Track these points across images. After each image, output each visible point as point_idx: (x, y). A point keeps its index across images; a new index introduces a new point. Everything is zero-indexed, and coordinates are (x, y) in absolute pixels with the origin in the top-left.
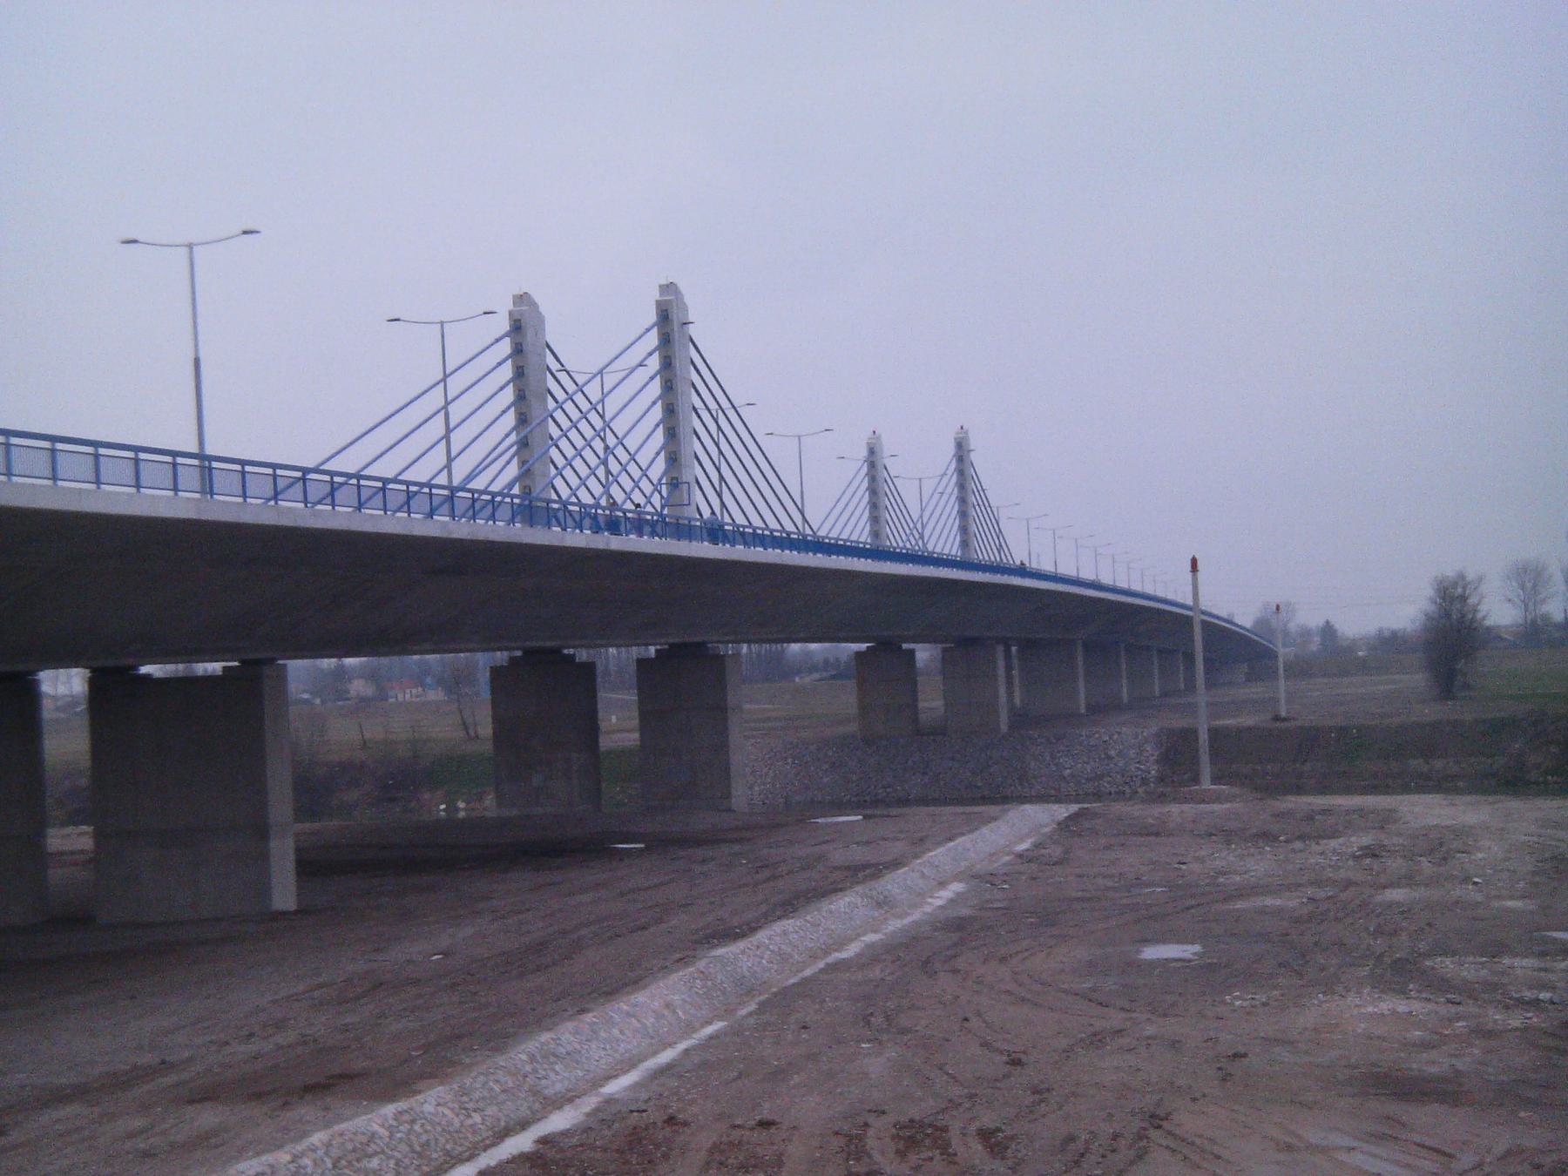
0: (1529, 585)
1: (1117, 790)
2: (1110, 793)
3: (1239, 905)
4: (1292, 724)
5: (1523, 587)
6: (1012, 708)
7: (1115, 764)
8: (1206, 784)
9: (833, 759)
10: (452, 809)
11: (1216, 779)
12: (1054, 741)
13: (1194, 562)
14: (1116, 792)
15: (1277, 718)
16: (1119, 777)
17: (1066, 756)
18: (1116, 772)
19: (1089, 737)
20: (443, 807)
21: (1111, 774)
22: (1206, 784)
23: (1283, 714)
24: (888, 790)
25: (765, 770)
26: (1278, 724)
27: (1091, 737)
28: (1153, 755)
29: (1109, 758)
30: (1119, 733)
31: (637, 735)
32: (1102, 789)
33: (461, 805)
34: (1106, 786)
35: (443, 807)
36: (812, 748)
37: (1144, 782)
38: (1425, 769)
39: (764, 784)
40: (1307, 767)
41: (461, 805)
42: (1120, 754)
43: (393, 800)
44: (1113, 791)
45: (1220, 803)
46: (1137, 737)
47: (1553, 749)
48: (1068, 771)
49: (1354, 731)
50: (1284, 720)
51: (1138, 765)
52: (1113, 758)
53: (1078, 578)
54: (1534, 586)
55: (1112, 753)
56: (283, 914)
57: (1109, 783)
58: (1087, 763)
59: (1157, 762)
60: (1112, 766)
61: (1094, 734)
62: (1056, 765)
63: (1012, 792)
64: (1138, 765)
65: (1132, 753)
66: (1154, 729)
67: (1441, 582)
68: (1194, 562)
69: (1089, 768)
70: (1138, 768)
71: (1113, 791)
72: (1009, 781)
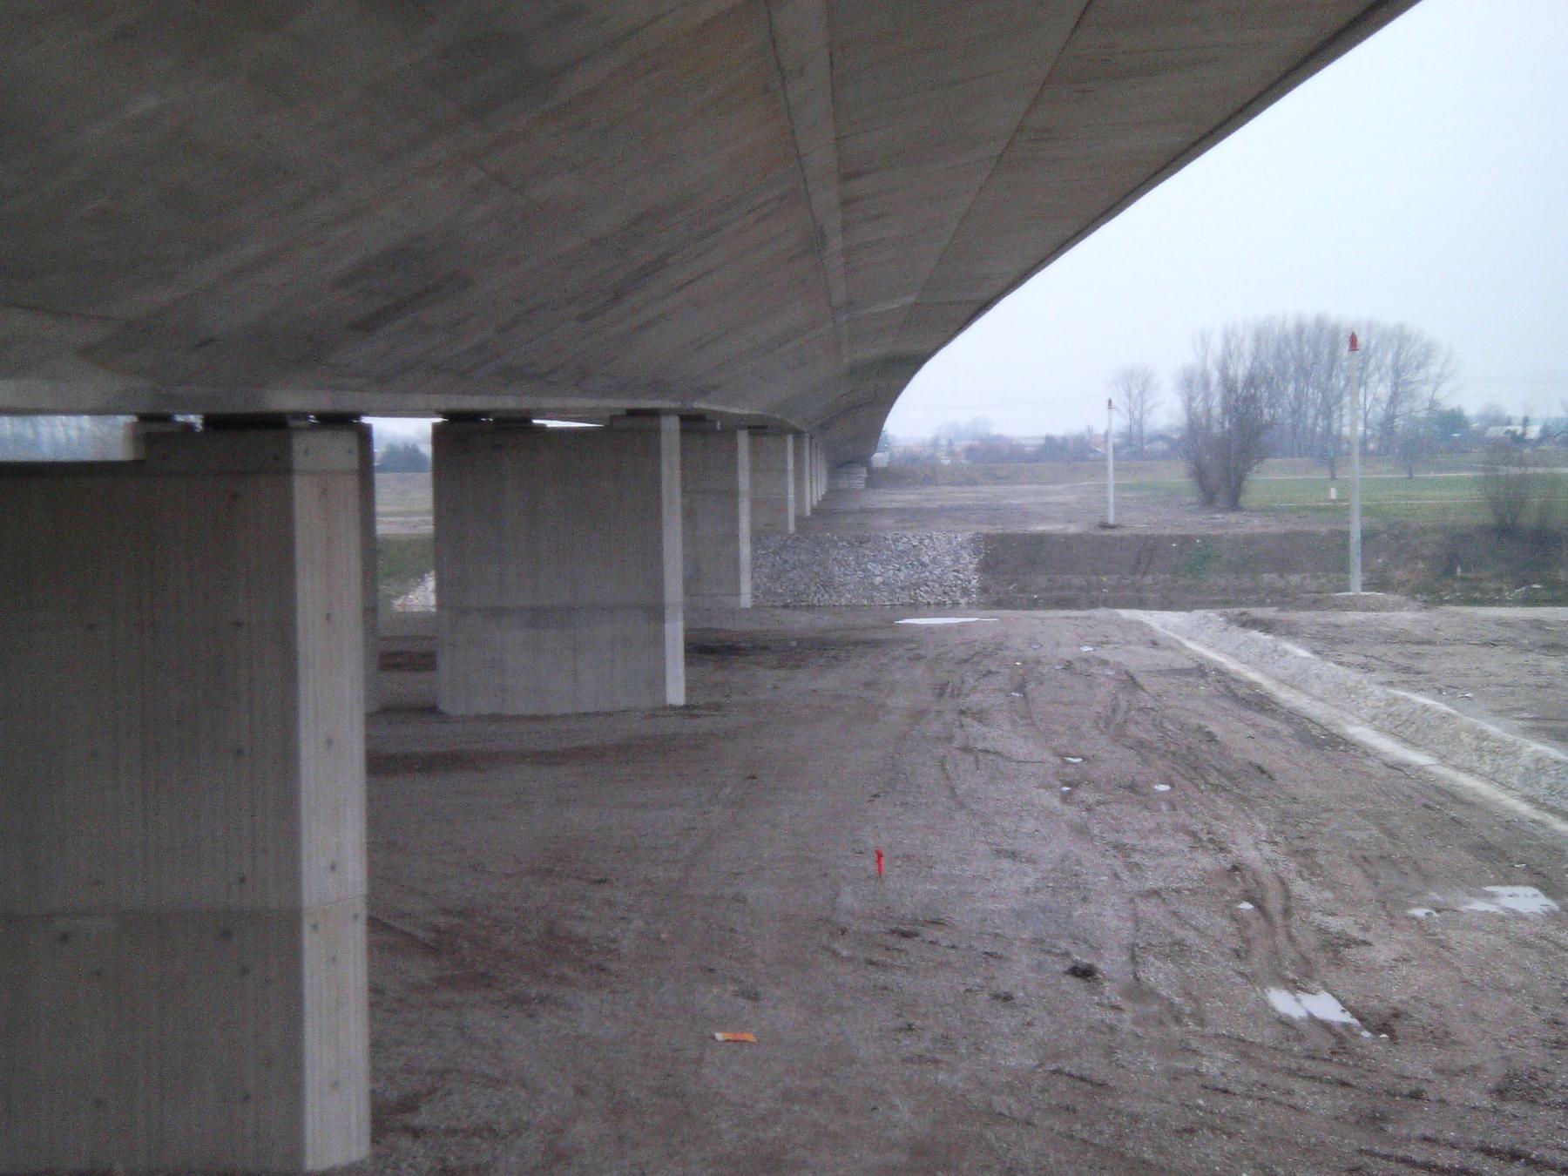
0: (1135, 392)
1: (936, 601)
4: (1117, 533)
5: (1129, 395)
6: (812, 506)
7: (931, 573)
8: (1356, 589)
11: (1367, 586)
15: (1105, 526)
16: (937, 586)
18: (933, 581)
19: (895, 541)
22: (1356, 589)
23: (1111, 521)
29: (923, 565)
30: (930, 538)
31: (431, 527)
32: (920, 598)
34: (924, 598)
37: (966, 592)
38: (1280, 584)
40: (1148, 580)
45: (1388, 611)
47: (1421, 565)
48: (878, 578)
49: (1198, 541)
50: (1113, 527)
52: (928, 565)
54: (1141, 394)
55: (926, 559)
56: (672, 707)
57: (926, 592)
58: (899, 570)
59: (977, 570)
60: (927, 574)
62: (863, 571)
65: (948, 561)
66: (969, 535)
69: (902, 576)
70: (956, 577)
71: (932, 601)
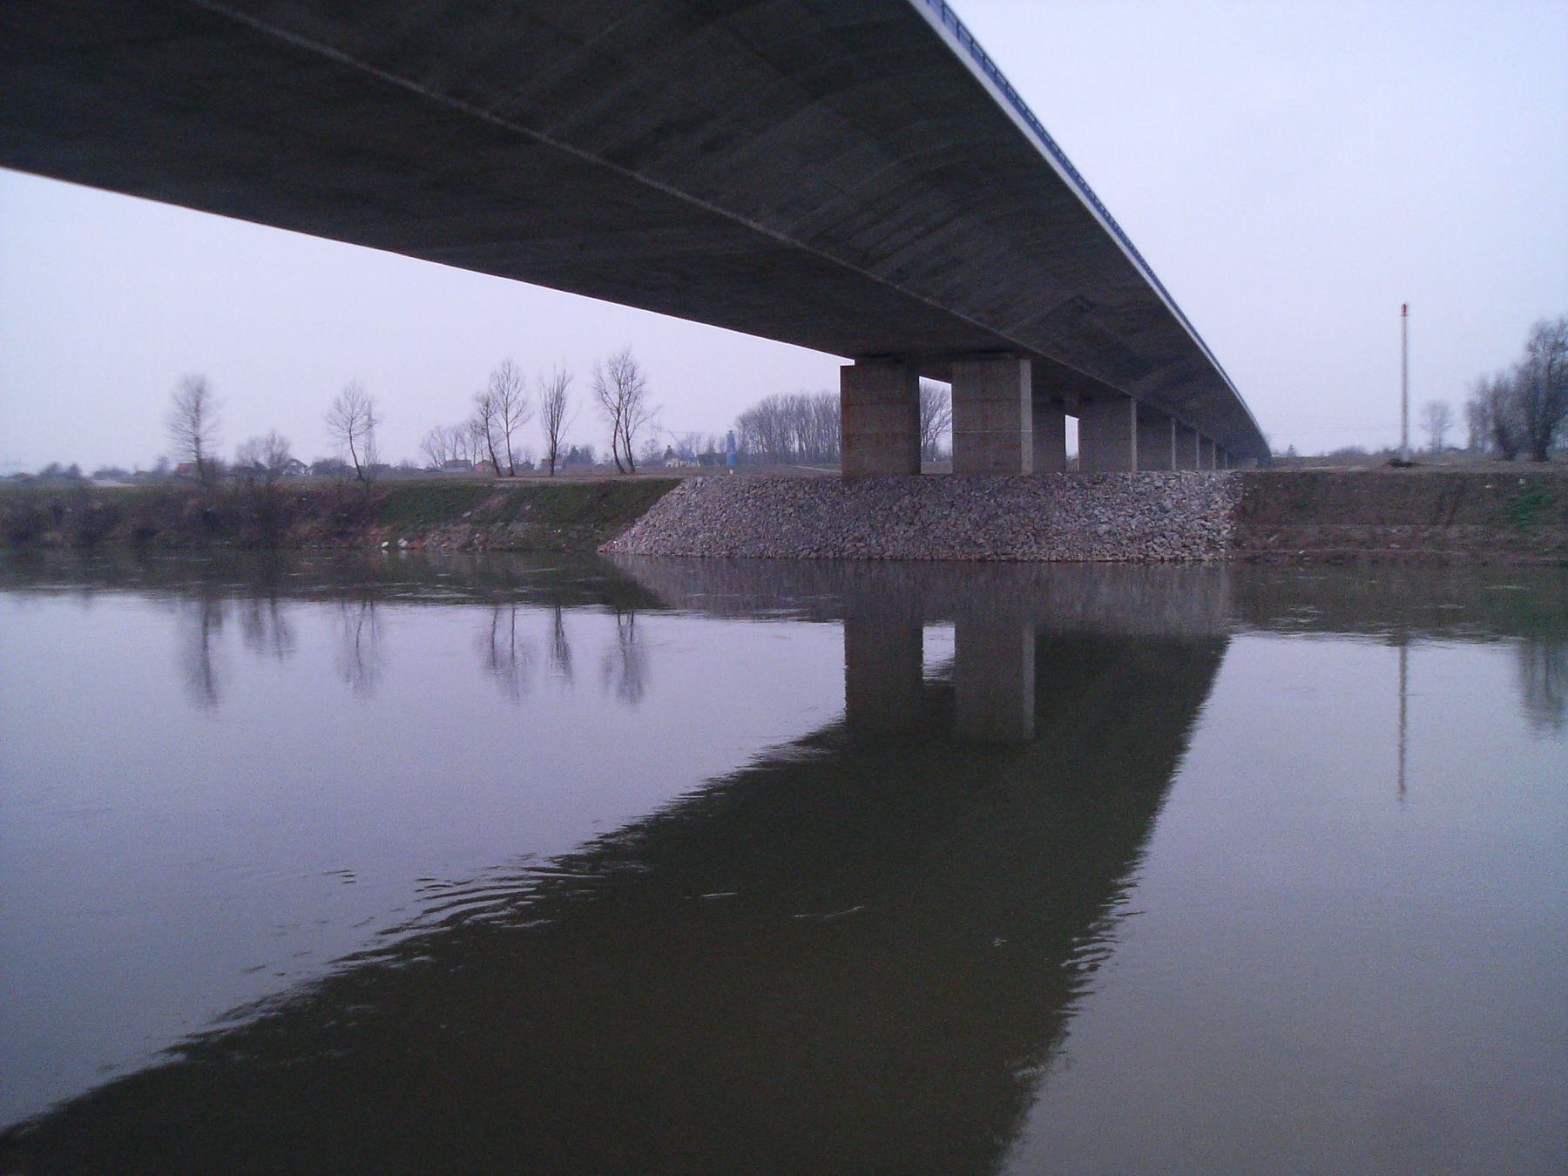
2: (1162, 560)
3: (459, 595)
4: (1412, 471)
7: (1171, 520)
9: (802, 502)
10: (393, 548)
12: (1089, 485)
13: (1405, 307)
14: (1170, 560)
17: (1104, 506)
20: (385, 544)
21: (1166, 533)
24: (859, 545)
25: (718, 513)
26: (1397, 471)
27: (1139, 481)
28: (1224, 509)
29: (1164, 510)
30: (1179, 478)
33: (403, 543)
35: (385, 544)
36: (781, 487)
39: (711, 530)
40: (1454, 532)
41: (403, 543)
42: (1178, 505)
43: (341, 534)
44: (1166, 557)
46: (1201, 484)
48: (1104, 526)
51: (1203, 522)
53: (206, 470)
55: (1168, 504)
60: (1167, 521)
61: (1143, 478)
62: (1089, 517)
63: (1024, 554)
64: (1203, 522)
65: (1195, 505)
67: (1542, 329)
68: (1405, 307)
69: (1134, 523)
71: (1166, 557)
72: (1022, 538)
